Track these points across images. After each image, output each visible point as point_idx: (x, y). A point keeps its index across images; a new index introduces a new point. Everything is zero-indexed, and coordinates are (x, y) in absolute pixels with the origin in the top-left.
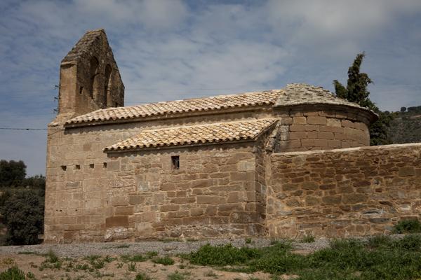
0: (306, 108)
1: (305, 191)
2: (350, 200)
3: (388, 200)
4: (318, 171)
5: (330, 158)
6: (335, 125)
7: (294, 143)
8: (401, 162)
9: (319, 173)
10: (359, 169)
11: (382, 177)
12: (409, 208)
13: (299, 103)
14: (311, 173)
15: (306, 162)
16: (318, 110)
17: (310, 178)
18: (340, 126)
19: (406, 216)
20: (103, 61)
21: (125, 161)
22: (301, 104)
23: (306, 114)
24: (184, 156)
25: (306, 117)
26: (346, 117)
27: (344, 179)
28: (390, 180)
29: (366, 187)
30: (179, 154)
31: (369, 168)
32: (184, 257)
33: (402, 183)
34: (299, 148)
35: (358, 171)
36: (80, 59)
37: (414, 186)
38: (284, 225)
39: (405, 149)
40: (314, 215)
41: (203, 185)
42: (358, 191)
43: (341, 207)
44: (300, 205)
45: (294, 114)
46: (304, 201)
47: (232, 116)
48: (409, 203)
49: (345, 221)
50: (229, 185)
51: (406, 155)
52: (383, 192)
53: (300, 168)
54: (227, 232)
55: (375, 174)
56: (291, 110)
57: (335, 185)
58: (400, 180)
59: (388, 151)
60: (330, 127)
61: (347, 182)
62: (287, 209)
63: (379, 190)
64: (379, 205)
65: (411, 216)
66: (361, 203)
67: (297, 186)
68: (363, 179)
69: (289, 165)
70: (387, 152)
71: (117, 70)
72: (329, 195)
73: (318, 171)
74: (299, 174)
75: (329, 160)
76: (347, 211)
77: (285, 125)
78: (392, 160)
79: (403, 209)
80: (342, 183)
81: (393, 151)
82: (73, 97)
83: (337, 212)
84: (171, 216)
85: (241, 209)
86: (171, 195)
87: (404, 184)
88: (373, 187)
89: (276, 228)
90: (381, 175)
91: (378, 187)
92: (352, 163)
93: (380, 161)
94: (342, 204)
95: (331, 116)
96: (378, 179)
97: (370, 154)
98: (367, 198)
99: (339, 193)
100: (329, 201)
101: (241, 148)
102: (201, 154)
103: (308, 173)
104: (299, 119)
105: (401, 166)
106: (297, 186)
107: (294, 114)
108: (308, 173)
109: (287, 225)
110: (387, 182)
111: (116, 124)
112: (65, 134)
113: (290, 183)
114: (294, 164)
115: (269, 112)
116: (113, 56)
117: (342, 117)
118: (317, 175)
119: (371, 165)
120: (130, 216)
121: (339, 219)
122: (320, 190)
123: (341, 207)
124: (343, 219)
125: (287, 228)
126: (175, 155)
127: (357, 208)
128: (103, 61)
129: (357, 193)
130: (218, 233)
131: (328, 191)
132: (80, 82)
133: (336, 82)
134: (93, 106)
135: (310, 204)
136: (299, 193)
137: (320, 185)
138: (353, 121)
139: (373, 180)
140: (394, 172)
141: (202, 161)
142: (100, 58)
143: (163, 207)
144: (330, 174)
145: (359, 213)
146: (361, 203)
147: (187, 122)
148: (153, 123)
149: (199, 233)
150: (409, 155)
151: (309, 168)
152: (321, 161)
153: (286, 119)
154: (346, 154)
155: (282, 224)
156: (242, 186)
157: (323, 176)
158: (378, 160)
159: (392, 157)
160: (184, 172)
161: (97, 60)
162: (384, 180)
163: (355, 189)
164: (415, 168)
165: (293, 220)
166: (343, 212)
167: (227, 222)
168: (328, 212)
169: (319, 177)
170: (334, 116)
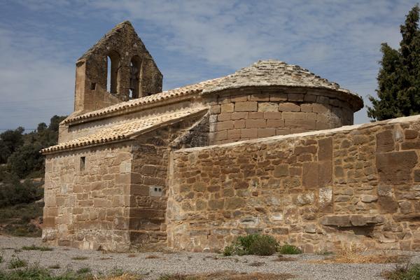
0: (261, 92)
1: (196, 193)
2: (231, 205)
3: (263, 207)
4: (207, 170)
5: (217, 155)
6: (271, 110)
7: (221, 135)
8: (277, 159)
9: (207, 173)
10: (239, 167)
11: (259, 178)
12: (280, 217)
13: (222, 88)
14: (202, 172)
15: (199, 159)
16: (247, 95)
17: (201, 178)
18: (276, 111)
19: (277, 227)
20: (127, 54)
21: (55, 162)
22: (225, 90)
23: (233, 100)
24: (89, 155)
25: (234, 103)
26: (285, 100)
27: (227, 180)
28: (266, 181)
29: (244, 190)
30: (85, 155)
31: (248, 167)
32: (201, 251)
33: (276, 185)
34: (226, 140)
35: (239, 171)
36: (91, 56)
37: (287, 189)
38: (178, 232)
39: (282, 141)
40: (202, 221)
41: (97, 187)
42: (238, 194)
43: (224, 213)
44: (191, 208)
45: (222, 101)
46: (195, 204)
47: (174, 106)
48: (281, 211)
49: (225, 229)
50: (114, 188)
51: (281, 150)
52: (259, 196)
53: (193, 167)
54: (110, 238)
55: (253, 173)
56: (218, 97)
57: (219, 187)
58: (274, 181)
59: (266, 145)
60: (263, 114)
61: (229, 183)
62: (182, 213)
63: (255, 194)
64: (255, 212)
65: (283, 227)
66: (239, 209)
67: (190, 187)
68: (243, 180)
69: (186, 163)
70: (264, 147)
71: (150, 59)
72: (214, 198)
73: (207, 170)
74: (193, 174)
75: (217, 157)
76: (228, 217)
77: (214, 114)
78: (268, 157)
79: (276, 218)
80: (225, 185)
81: (270, 145)
82: (83, 94)
83: (219, 219)
84: (79, 219)
85: (121, 214)
86: (79, 197)
87: (278, 187)
88: (251, 189)
89: (172, 234)
90: (259, 174)
91: (255, 189)
92: (234, 161)
93: (259, 157)
94: (224, 209)
95: (264, 100)
96: (256, 180)
97: (249, 149)
98: (245, 203)
99: (223, 196)
100: (214, 205)
101: (123, 148)
102: (99, 155)
103: (199, 172)
104: (227, 106)
105: (276, 163)
106: (190, 187)
107: (222, 101)
108: (199, 172)
109: (179, 232)
110: (263, 183)
111: (97, 120)
112: (69, 132)
113: (186, 183)
114: (189, 162)
115: (199, 100)
116: (143, 46)
117: (278, 99)
118: (273, 162)
119: (251, 163)
120: (56, 218)
121: (221, 227)
122: (208, 192)
123: (224, 213)
124: (225, 227)
125: (181, 235)
126: (83, 156)
127: (237, 214)
128: (127, 54)
129: (237, 197)
130: (105, 240)
131: (214, 193)
132: (91, 78)
133: (385, 45)
134: (111, 100)
135: (199, 208)
136: (191, 196)
137: (208, 186)
138: (298, 103)
139: (251, 182)
140: (269, 172)
141: (99, 162)
142: (122, 51)
143: (74, 210)
144: (216, 175)
145: (238, 221)
146: (239, 209)
147: (152, 114)
148: (121, 118)
149: (94, 238)
150: (284, 150)
151: (200, 167)
152: (210, 158)
153: (215, 107)
154: (230, 149)
155: (177, 230)
156: (122, 189)
157: (212, 176)
158: (256, 156)
159: (269, 153)
160: (87, 174)
161: (118, 53)
162: (260, 182)
163: (235, 192)
164: (290, 166)
165: (185, 226)
166: (225, 219)
167: (111, 228)
168: (212, 218)
169: (208, 177)
170: (267, 99)
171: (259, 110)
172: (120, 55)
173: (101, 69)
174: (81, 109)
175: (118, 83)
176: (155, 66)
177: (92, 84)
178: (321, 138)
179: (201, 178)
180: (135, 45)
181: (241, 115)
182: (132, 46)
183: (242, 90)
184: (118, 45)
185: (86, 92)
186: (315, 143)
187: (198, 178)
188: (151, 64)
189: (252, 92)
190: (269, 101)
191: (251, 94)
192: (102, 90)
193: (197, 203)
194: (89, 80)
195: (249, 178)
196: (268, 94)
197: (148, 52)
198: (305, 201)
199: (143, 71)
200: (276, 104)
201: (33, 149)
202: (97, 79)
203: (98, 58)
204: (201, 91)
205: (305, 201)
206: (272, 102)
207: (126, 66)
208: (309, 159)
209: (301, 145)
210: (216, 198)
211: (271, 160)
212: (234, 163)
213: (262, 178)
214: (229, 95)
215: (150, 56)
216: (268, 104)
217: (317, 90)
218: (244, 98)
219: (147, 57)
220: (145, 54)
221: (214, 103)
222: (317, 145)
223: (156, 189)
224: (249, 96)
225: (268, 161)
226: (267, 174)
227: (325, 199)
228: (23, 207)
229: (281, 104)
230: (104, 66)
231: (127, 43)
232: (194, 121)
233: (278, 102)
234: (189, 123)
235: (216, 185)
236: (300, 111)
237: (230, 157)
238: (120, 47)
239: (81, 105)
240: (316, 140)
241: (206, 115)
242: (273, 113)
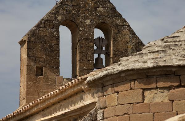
6: (158, 100)
16: (131, 81)
18: (166, 100)
23: (116, 89)
25: (118, 93)
45: (106, 91)
77: (102, 109)
95: (150, 87)
116: (114, 9)
117: (168, 84)
132: (35, 61)
170: (154, 85)
171: (146, 101)
172: (77, 25)
173: (50, 46)
174: (24, 102)
175: (78, 63)
176: (133, 33)
180: (100, 9)
183: (123, 75)
184: (74, 12)
185: (29, 80)
188: (125, 31)
189: (135, 77)
190: (157, 88)
191: (134, 80)
192: (52, 75)
194: (33, 64)
196: (154, 78)
197: (120, 16)
199: (114, 43)
200: (166, 91)
202: (44, 61)
203: (46, 33)
206: (160, 88)
207: (87, 39)
214: (111, 82)
215: (124, 21)
216: (155, 91)
218: (127, 86)
219: (119, 22)
220: (115, 19)
221: (100, 94)
224: (133, 83)
229: (172, 91)
230: (55, 42)
231: (88, 7)
233: (169, 88)
238: (78, 15)
239: (24, 99)
241: (92, 111)
242: (163, 103)
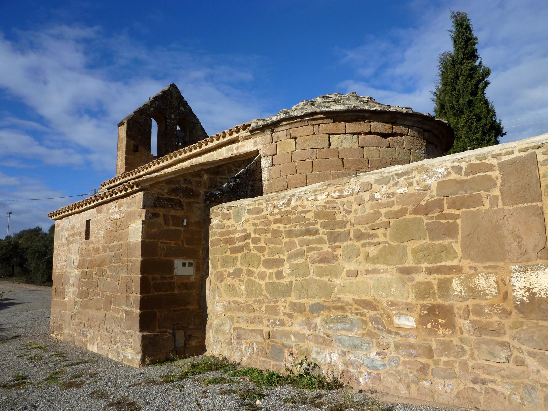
6: (346, 145)
8: (396, 208)
14: (253, 235)
20: (173, 116)
28: (373, 251)
74: (239, 239)
82: (124, 156)
92: (307, 216)
93: (355, 206)
128: (173, 116)
131: (273, 270)
137: (263, 259)
177: (134, 146)
178: (504, 158)
179: (252, 246)
181: (307, 154)
182: (179, 109)
186: (490, 168)
187: (248, 245)
193: (247, 286)
195: (337, 244)
198: (471, 290)
201: (356, 262)
204: (249, 125)
205: (471, 290)
208: (479, 202)
209: (454, 176)
210: (278, 278)
211: (383, 211)
212: (309, 219)
213: (364, 245)
217: (409, 118)
222: (495, 174)
223: (184, 265)
225: (378, 213)
226: (376, 236)
227: (528, 290)
228: (419, 190)
232: (240, 166)
234: (234, 168)
235: (277, 257)
236: (389, 147)
237: (300, 209)
240: (495, 162)
